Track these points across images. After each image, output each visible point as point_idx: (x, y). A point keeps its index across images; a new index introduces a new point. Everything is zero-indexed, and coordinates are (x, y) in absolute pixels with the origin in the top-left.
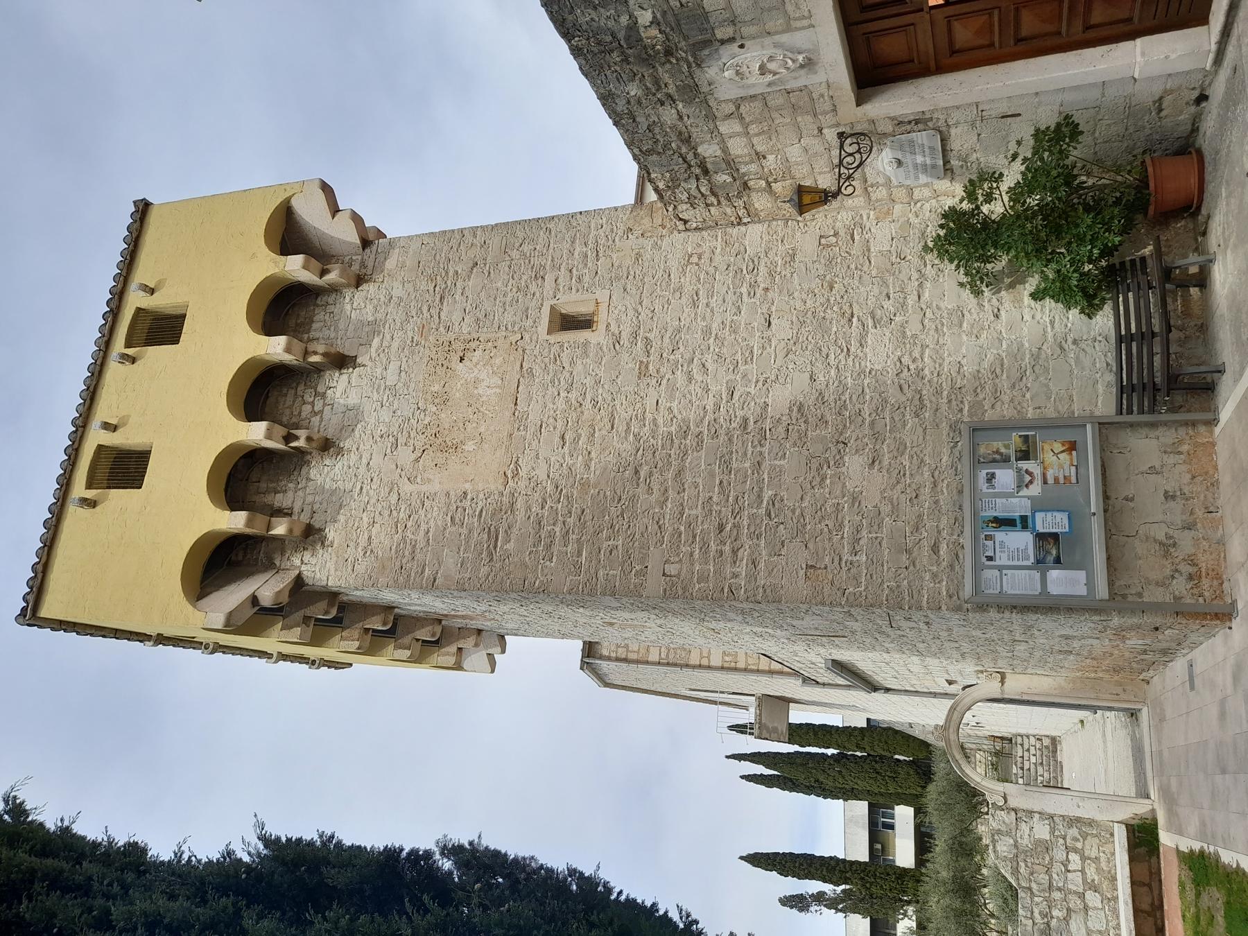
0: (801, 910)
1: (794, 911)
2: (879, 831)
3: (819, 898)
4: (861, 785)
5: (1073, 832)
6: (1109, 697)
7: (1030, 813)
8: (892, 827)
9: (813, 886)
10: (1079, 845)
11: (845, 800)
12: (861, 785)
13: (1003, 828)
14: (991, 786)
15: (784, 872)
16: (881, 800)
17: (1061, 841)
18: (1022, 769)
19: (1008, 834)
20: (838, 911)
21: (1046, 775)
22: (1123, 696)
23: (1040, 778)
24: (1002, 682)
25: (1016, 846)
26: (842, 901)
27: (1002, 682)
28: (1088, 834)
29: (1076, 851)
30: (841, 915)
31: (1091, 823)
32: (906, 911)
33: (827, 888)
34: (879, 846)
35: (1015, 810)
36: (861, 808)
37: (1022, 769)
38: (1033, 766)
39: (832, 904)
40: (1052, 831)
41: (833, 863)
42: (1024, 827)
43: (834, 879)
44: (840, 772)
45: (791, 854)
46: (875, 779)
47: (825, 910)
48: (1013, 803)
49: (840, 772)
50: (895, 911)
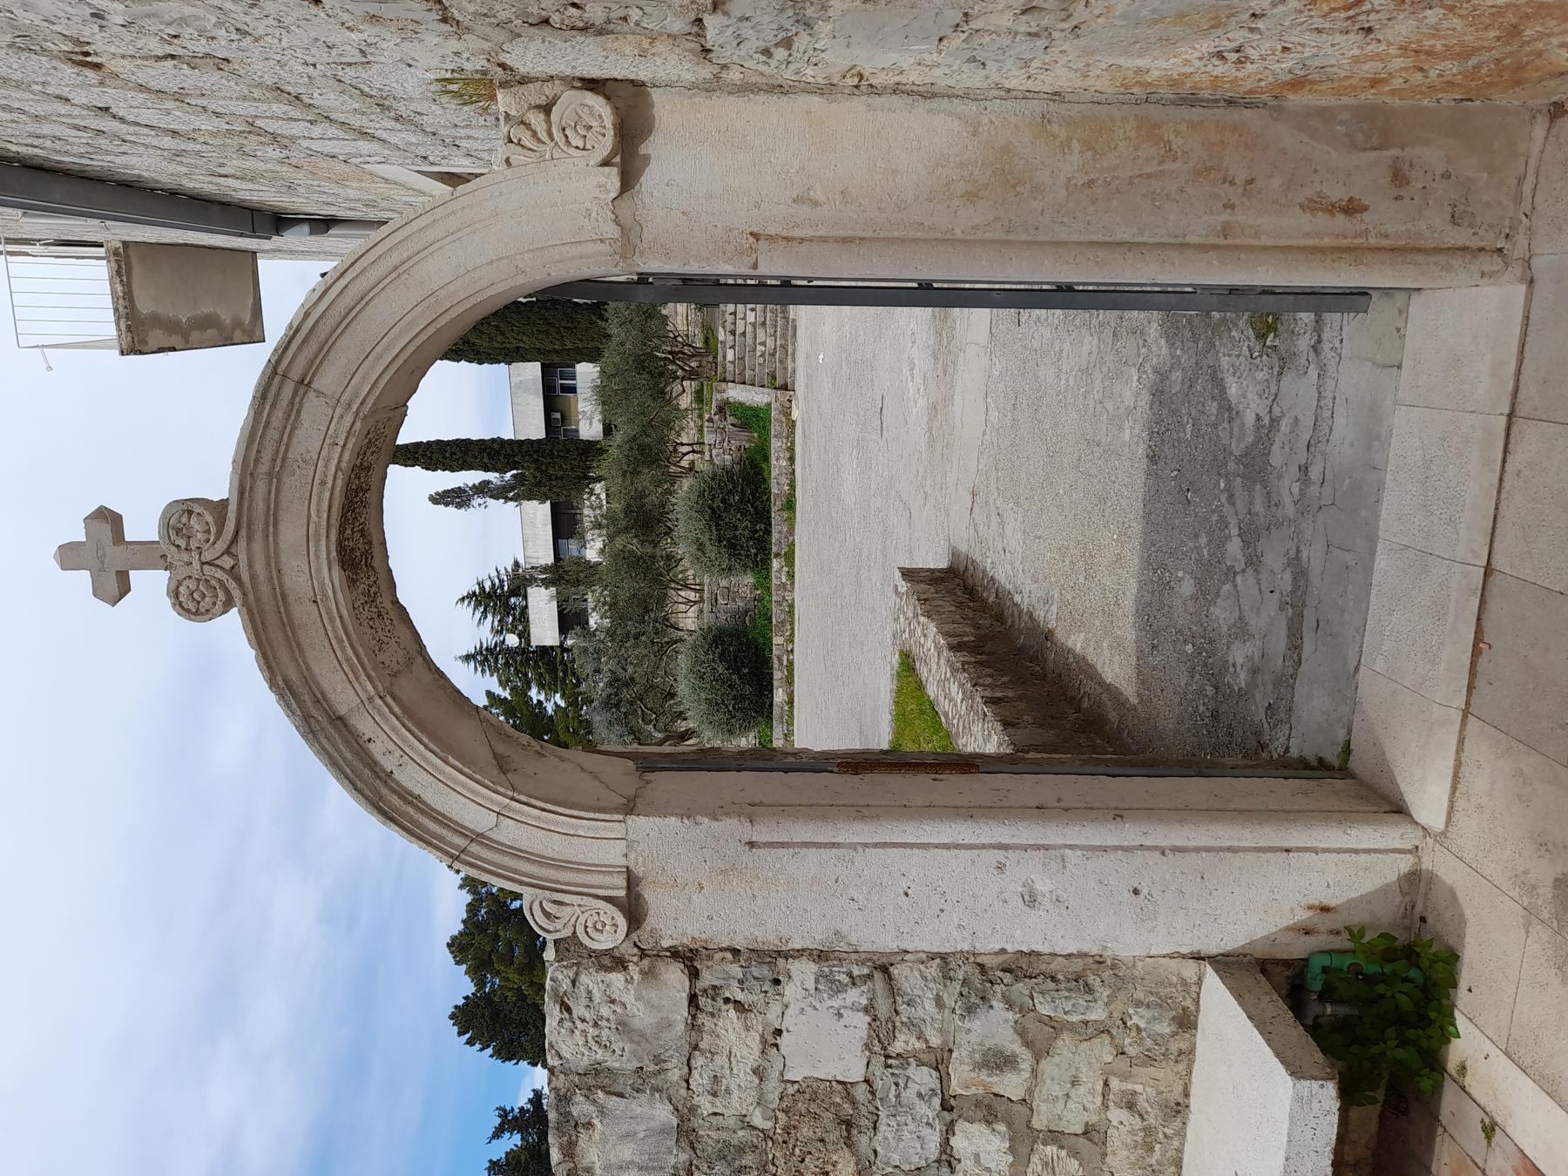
0: (459, 506)
1: (451, 509)
2: (555, 397)
3: (482, 489)
4: (527, 343)
5: (995, 1026)
6: (1297, 225)
7: (769, 962)
8: (573, 390)
9: (471, 477)
10: (1011, 1085)
11: (509, 363)
12: (527, 343)
13: (621, 1059)
14: (553, 846)
15: (430, 465)
16: (556, 359)
17: (924, 1078)
18: (733, 333)
19: (645, 1081)
20: (507, 499)
21: (770, 344)
22: (1386, 220)
23: (760, 348)
24: (627, 157)
25: (685, 1132)
26: (512, 489)
27: (627, 157)
28: (1057, 1027)
29: (990, 1110)
30: (512, 504)
31: (1084, 973)
32: (592, 490)
33: (492, 476)
34: (558, 415)
35: (689, 958)
36: (532, 370)
37: (733, 333)
38: (749, 329)
39: (500, 493)
40: (880, 1038)
41: (496, 446)
42: (733, 1037)
43: (500, 466)
44: (497, 327)
45: (438, 442)
46: (547, 333)
47: (491, 502)
48: (673, 921)
49: (497, 327)
50: (580, 491)
